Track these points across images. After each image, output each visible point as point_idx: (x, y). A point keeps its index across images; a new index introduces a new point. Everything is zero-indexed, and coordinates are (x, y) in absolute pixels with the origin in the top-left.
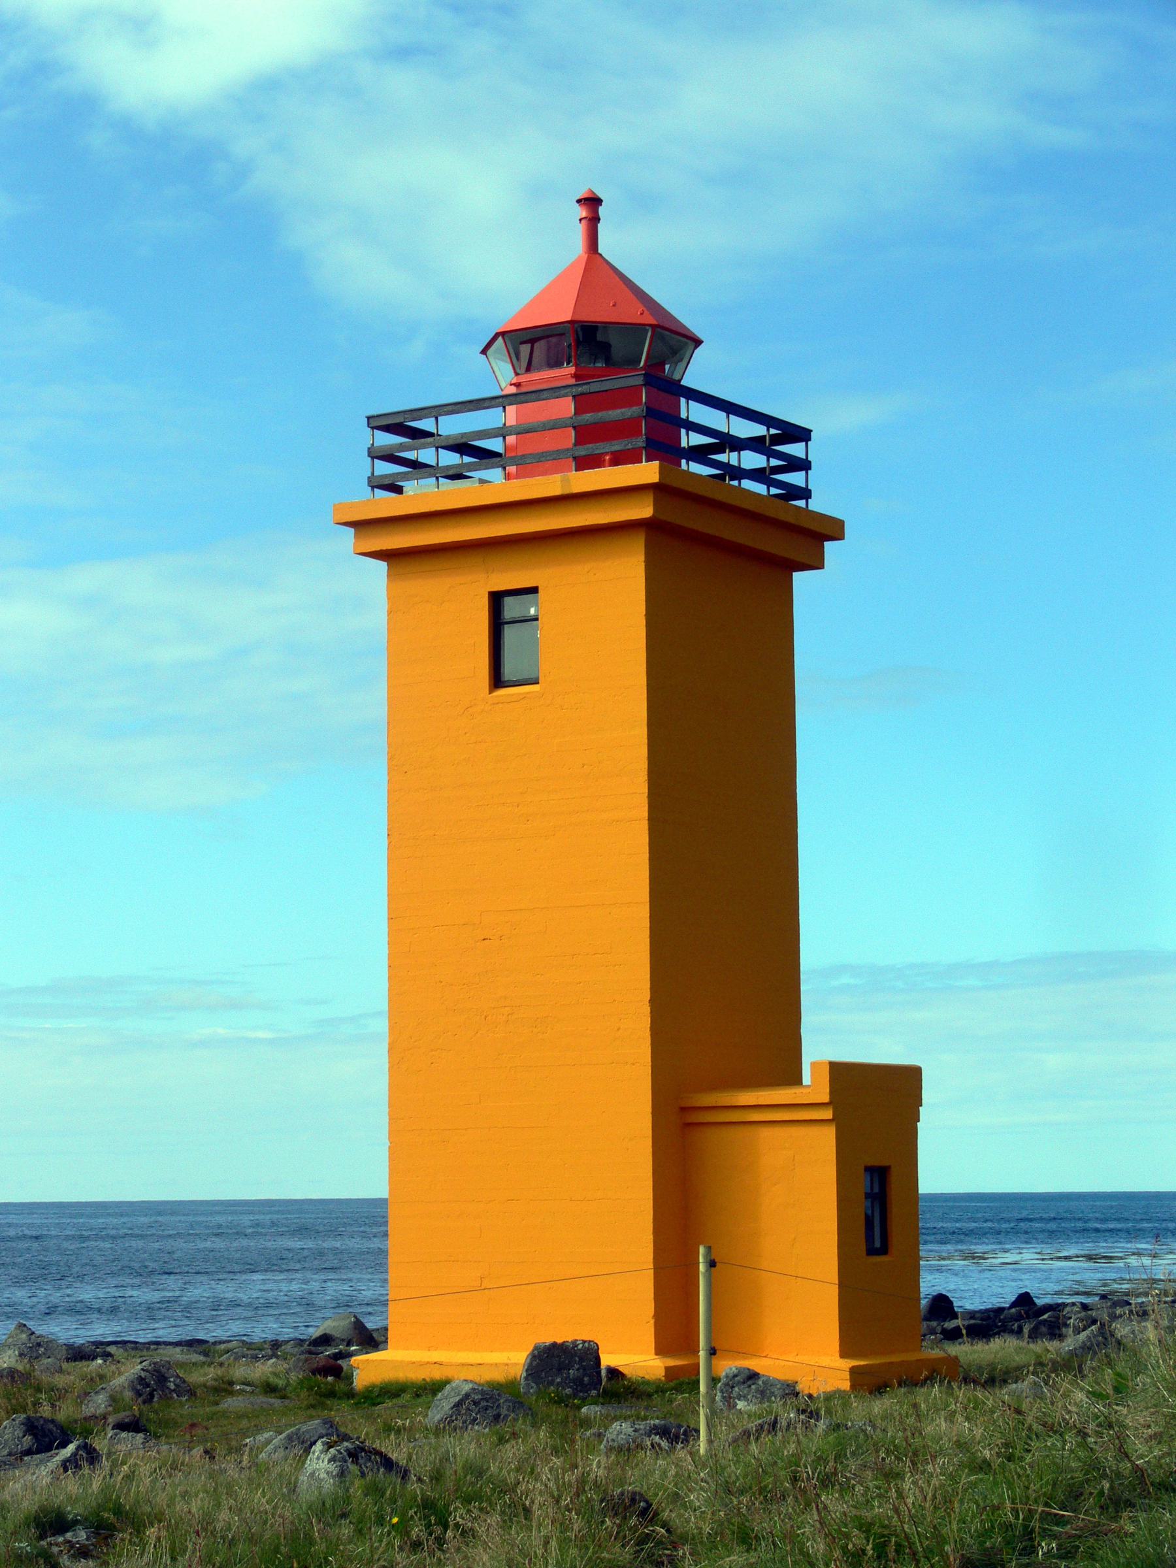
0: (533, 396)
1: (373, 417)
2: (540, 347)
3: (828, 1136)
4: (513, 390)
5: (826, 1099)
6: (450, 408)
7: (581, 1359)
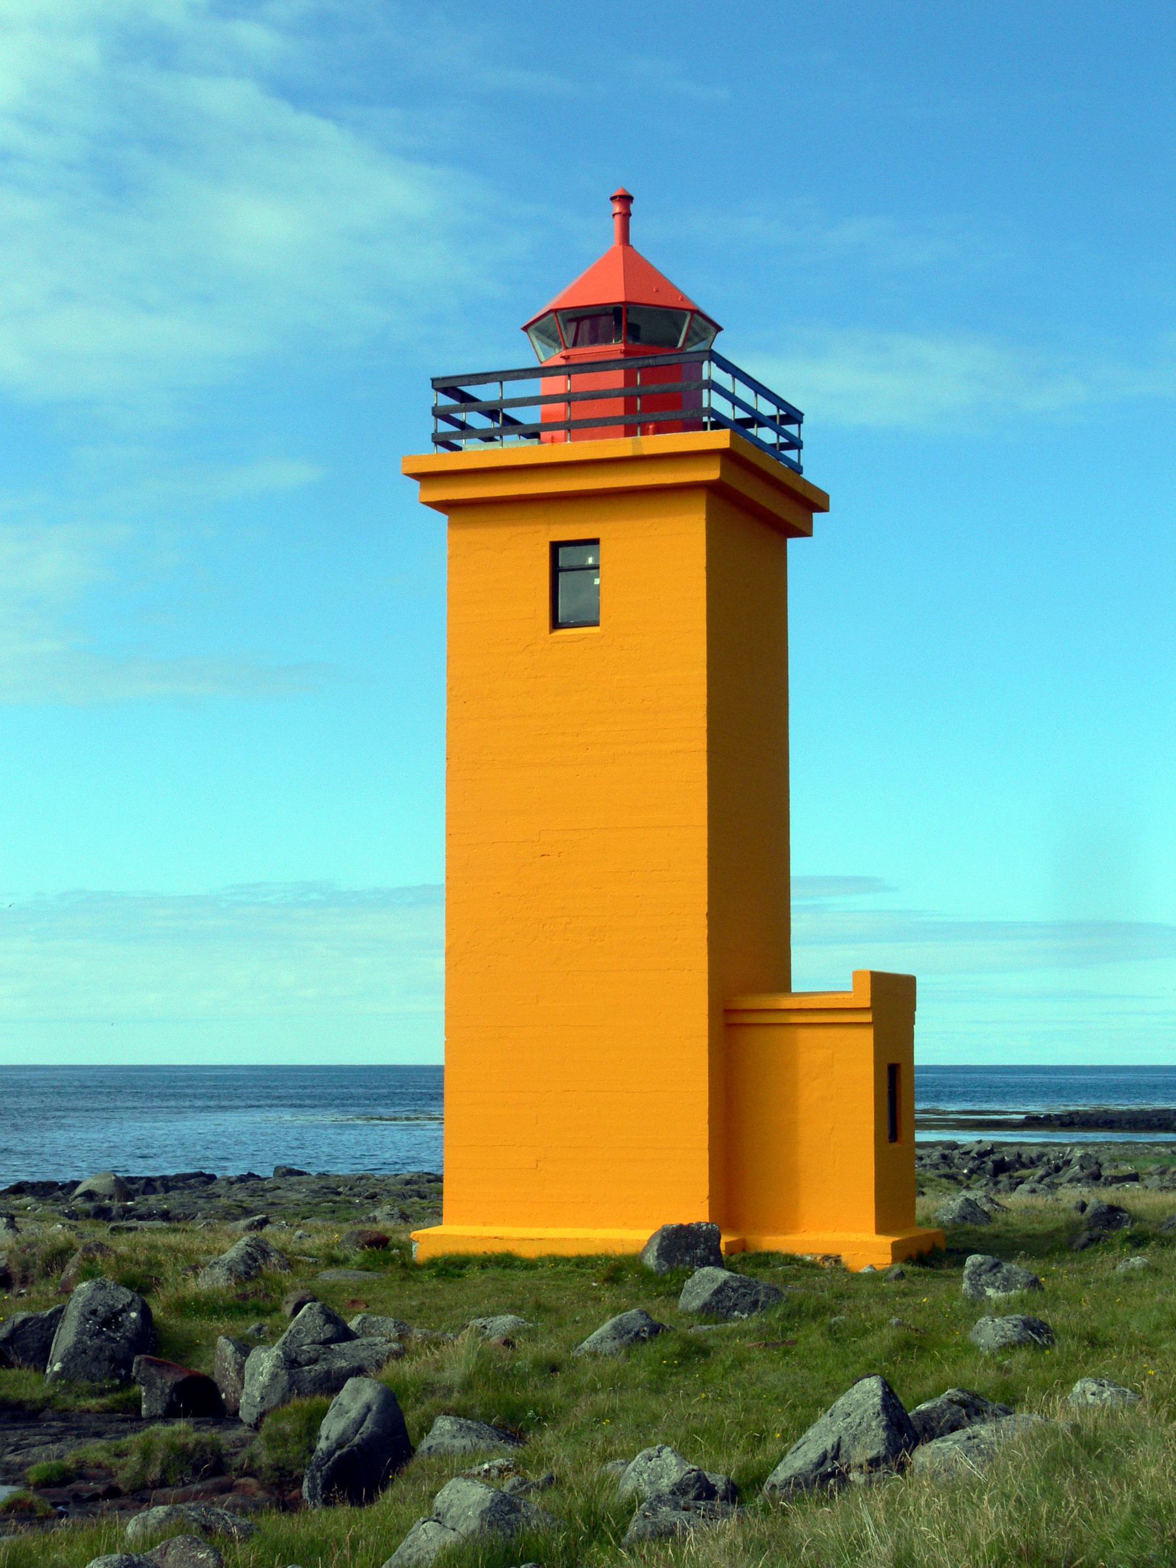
0: (589, 367)
1: (438, 379)
2: (586, 325)
3: (868, 1035)
4: (563, 362)
5: (868, 1004)
6: (516, 374)
7: (706, 1241)
